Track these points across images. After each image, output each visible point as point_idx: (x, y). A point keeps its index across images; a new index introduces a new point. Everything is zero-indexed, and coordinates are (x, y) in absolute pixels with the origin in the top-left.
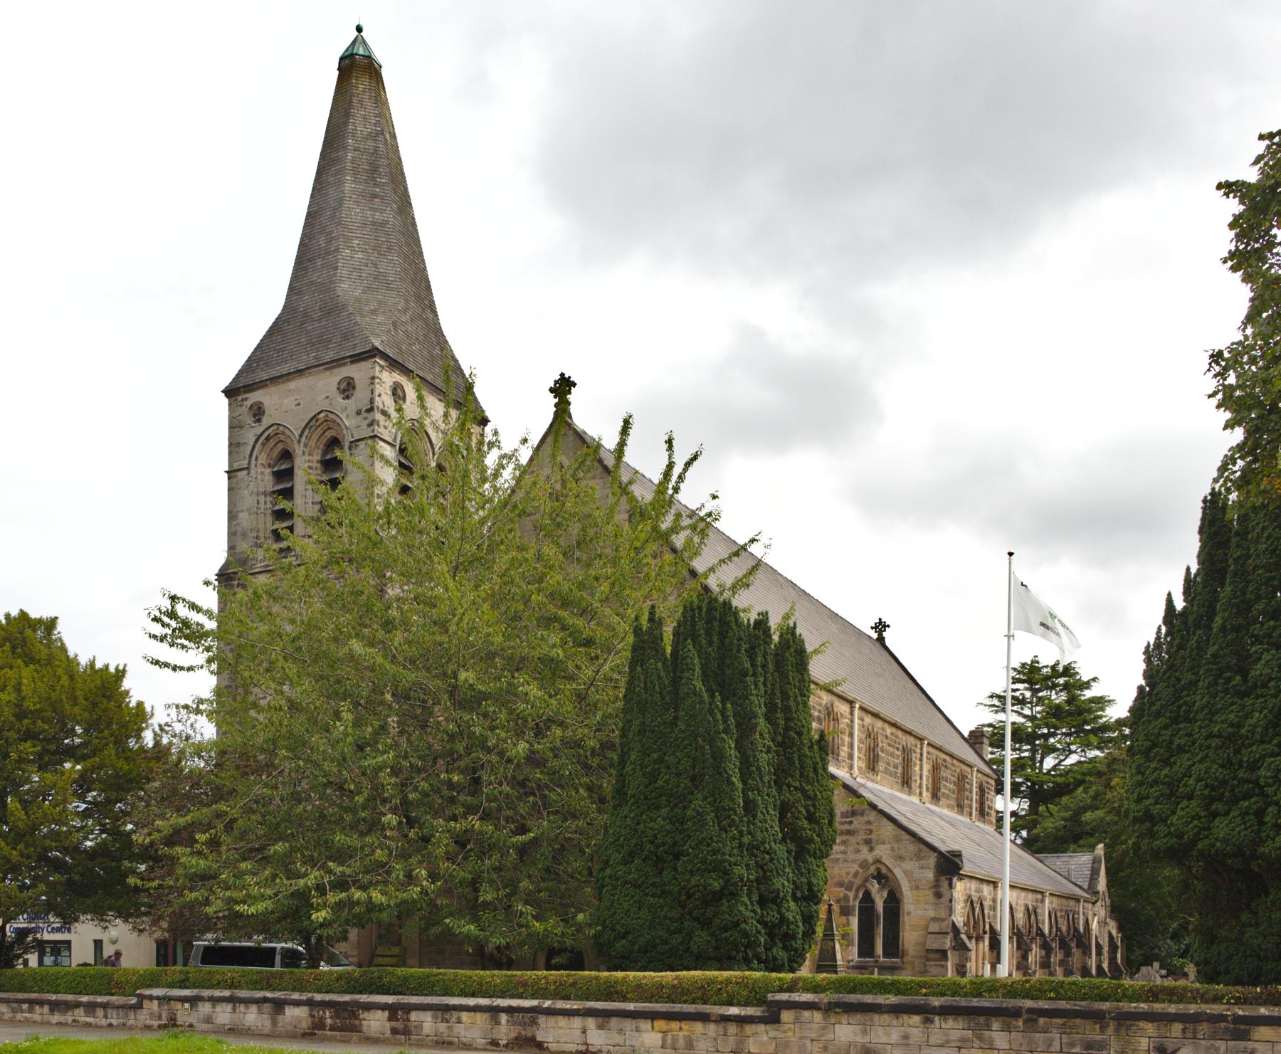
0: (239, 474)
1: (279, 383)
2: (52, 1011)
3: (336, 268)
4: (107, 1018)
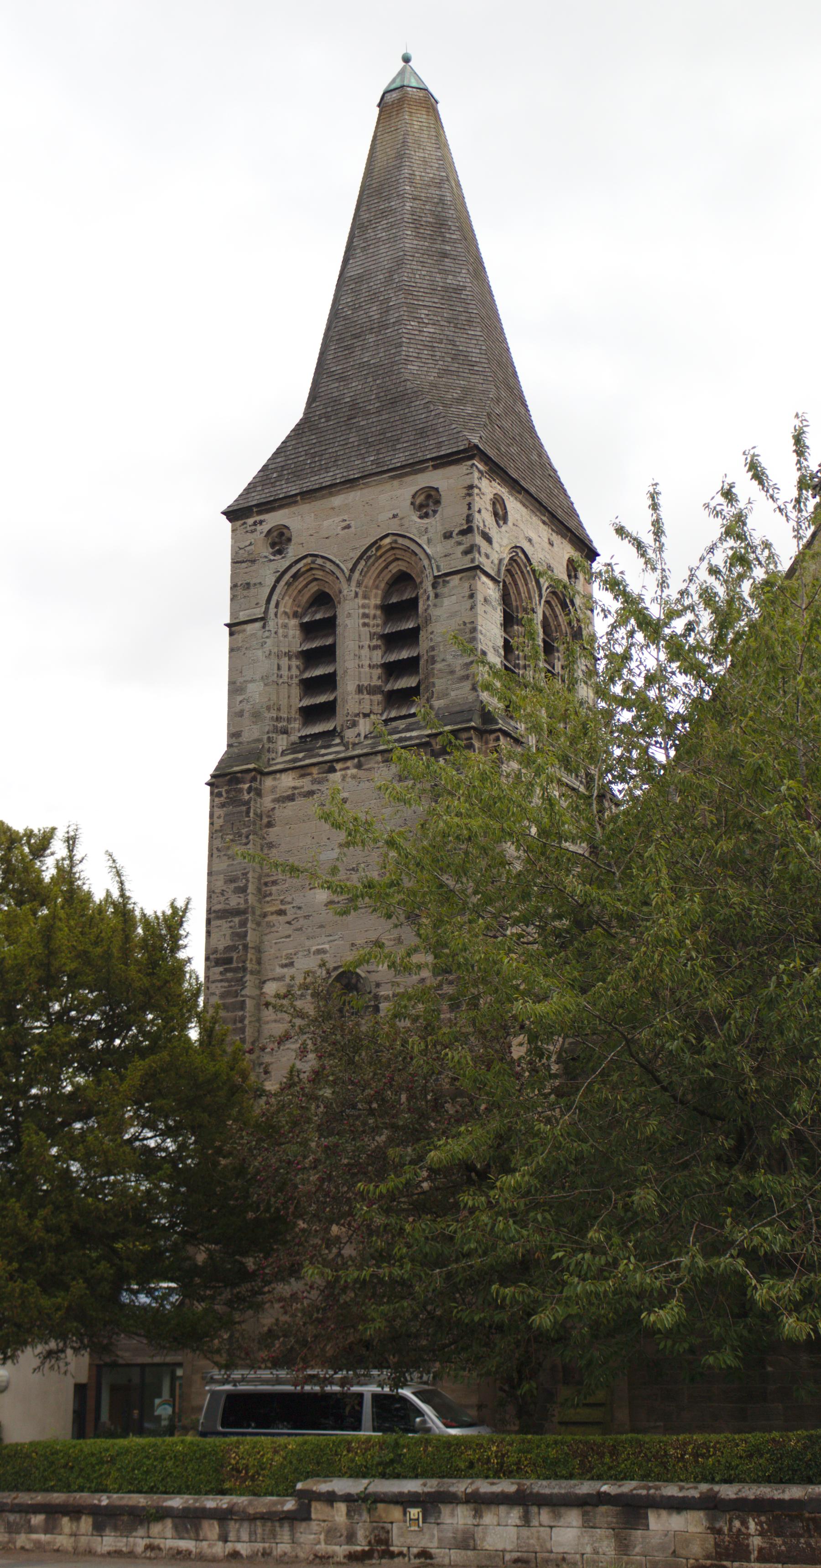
0: (249, 628)
1: (317, 499)
2: (99, 1528)
3: (400, 345)
4: (226, 1541)
